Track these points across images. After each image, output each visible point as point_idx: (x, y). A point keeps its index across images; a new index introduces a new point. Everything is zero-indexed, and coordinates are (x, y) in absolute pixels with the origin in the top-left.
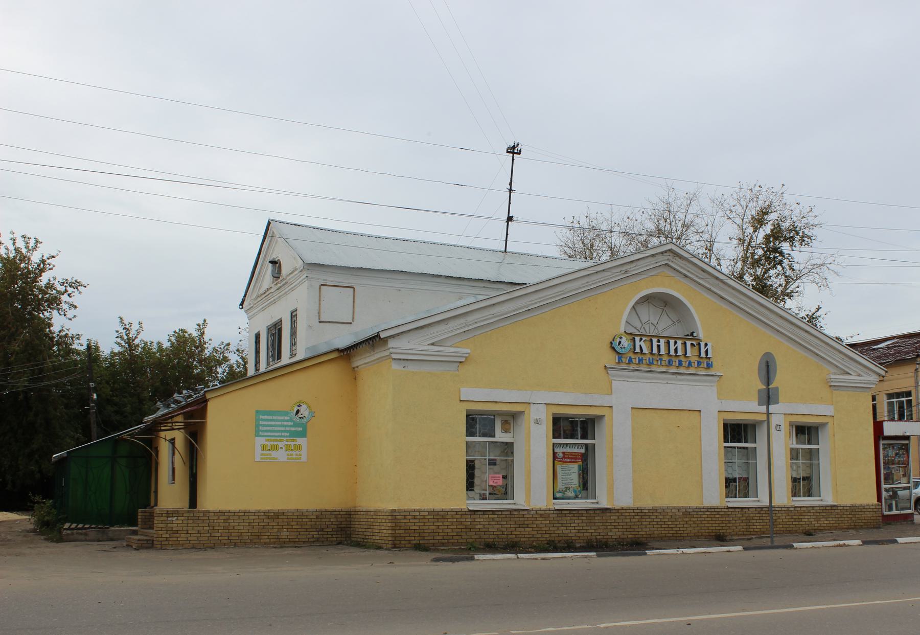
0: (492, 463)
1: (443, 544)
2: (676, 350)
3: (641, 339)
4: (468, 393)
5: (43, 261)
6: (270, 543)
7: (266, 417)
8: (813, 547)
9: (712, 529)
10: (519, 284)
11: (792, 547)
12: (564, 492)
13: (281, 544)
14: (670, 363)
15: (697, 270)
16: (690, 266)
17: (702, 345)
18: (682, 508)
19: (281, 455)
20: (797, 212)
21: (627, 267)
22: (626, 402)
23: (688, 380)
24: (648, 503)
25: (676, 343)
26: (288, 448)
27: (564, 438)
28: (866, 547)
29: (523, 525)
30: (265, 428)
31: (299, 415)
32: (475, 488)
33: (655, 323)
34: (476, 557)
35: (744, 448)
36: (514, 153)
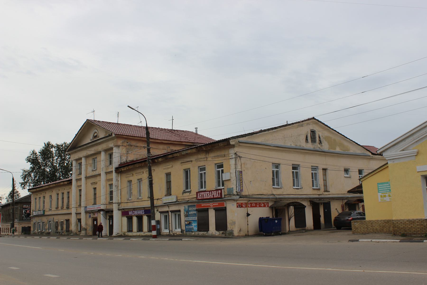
1: (414, 234)
4: (420, 168)
6: (387, 232)
11: (358, 241)
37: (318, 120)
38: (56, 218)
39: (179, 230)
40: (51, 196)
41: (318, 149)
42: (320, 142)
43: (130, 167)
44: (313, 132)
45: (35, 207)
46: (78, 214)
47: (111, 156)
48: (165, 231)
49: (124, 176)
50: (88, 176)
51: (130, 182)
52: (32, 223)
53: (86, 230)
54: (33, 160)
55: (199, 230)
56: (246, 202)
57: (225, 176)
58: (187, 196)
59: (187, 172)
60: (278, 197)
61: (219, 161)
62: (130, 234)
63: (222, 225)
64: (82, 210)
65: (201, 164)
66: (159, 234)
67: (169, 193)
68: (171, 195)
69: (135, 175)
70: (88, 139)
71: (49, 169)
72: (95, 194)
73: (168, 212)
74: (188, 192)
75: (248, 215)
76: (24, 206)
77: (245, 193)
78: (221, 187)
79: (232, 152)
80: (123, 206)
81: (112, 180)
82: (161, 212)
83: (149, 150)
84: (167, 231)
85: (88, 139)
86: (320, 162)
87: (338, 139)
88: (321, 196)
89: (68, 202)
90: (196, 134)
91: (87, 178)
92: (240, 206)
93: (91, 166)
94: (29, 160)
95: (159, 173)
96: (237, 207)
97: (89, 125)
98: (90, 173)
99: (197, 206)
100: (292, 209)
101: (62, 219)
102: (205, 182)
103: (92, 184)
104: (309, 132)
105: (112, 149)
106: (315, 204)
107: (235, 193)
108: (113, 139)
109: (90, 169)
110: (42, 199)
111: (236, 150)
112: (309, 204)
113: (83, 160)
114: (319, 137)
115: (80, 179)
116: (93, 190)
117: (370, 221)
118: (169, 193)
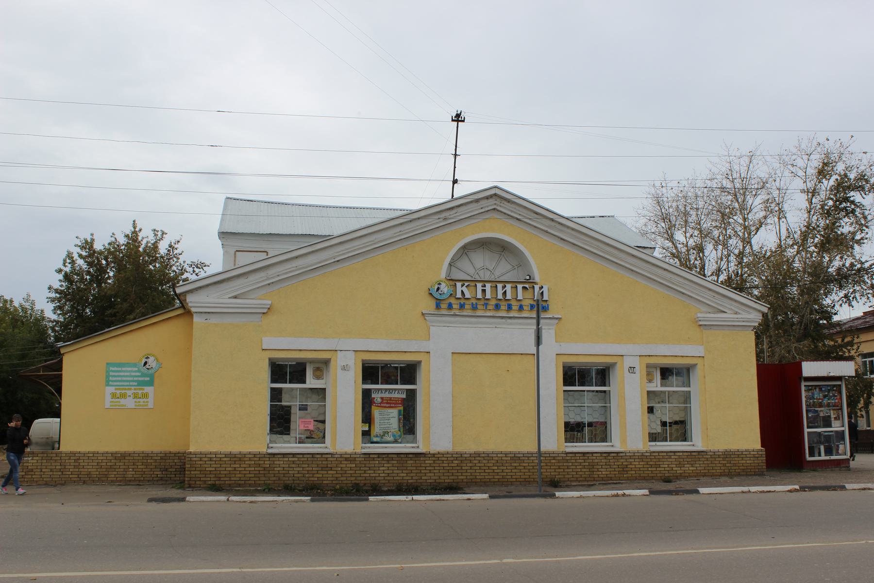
0: (303, 408)
1: (240, 485)
2: (505, 293)
3: (462, 286)
4: (270, 342)
5: (170, 246)
7: (116, 369)
8: (251, 502)
9: (540, 476)
10: (325, 236)
11: (843, 488)
12: (382, 437)
13: (125, 482)
14: (497, 307)
15: (529, 213)
16: (521, 209)
17: (537, 288)
19: (130, 403)
20: (865, 162)
22: (444, 349)
23: (520, 324)
24: (469, 447)
26: (135, 396)
27: (596, 385)
30: (114, 379)
31: (147, 366)
32: (292, 433)
33: (491, 268)
34: (557, 494)
35: (601, 391)
36: (458, 121)
102: (320, 262)
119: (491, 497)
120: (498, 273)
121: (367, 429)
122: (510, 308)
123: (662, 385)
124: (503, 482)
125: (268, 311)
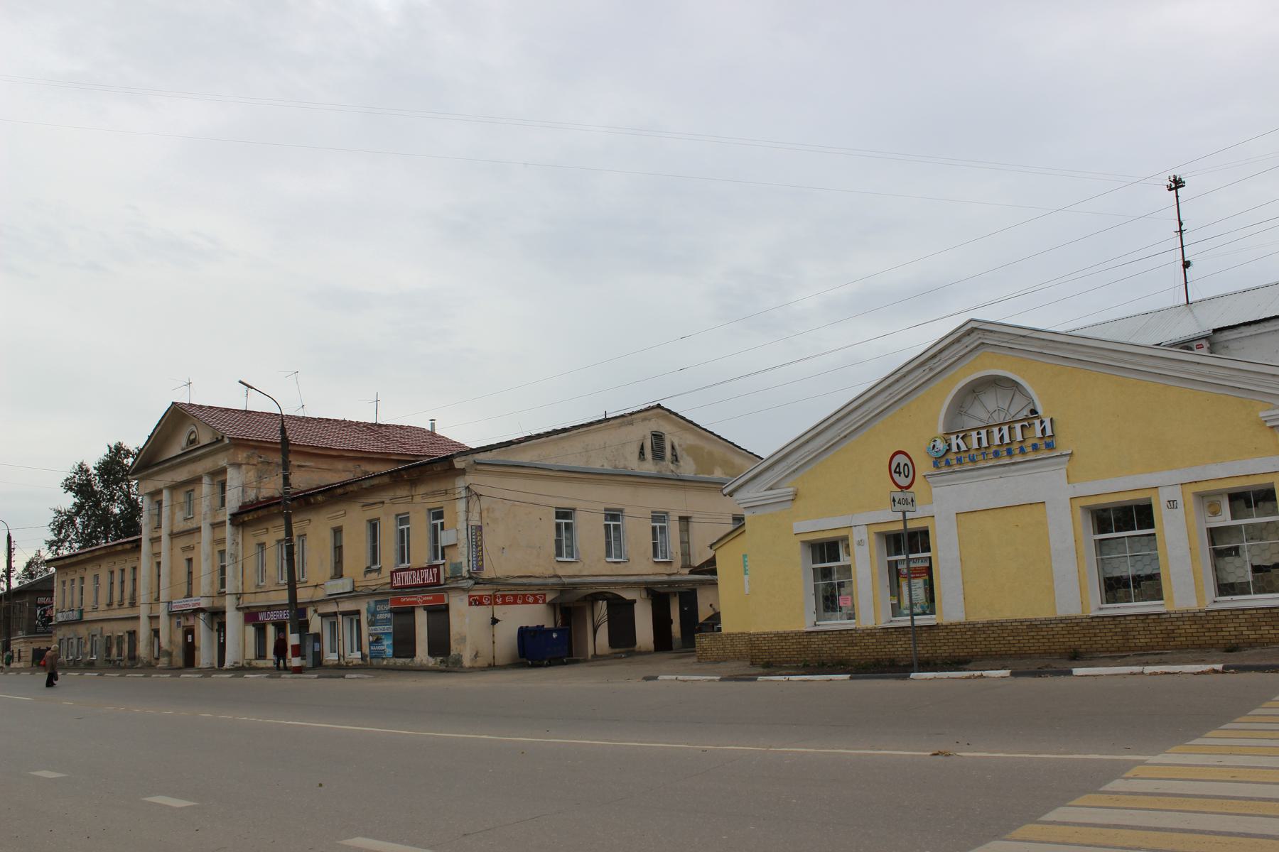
2: (1002, 438)
9: (1042, 649)
11: (655, 678)
18: (1026, 620)
21: (930, 364)
22: (943, 505)
25: (1000, 430)
28: (1232, 677)
29: (853, 644)
37: (669, 411)
38: (109, 629)
39: (358, 655)
40: (97, 577)
41: (669, 474)
42: (675, 459)
43: (260, 513)
44: (658, 437)
45: (62, 603)
46: (153, 618)
47: (223, 485)
48: (330, 658)
49: (250, 532)
50: (175, 530)
51: (262, 545)
52: (55, 639)
53: (169, 654)
54: (80, 486)
55: (396, 655)
56: (491, 593)
57: (445, 538)
58: (374, 581)
59: (374, 525)
60: (566, 580)
61: (435, 503)
62: (261, 663)
63: (440, 644)
64: (162, 610)
65: (401, 509)
66: (318, 662)
67: (338, 574)
68: (341, 576)
69: (271, 530)
70: (176, 449)
71: (106, 507)
72: (190, 573)
73: (335, 614)
74: (375, 570)
75: (495, 621)
76: (40, 600)
77: (486, 574)
78: (440, 561)
79: (461, 483)
80: (249, 601)
81: (223, 541)
82: (323, 616)
83: (286, 479)
84: (334, 657)
85: (176, 449)
86: (674, 502)
87: (718, 450)
88: (673, 578)
89: (134, 590)
90: (433, 434)
91: (173, 536)
92: (477, 602)
93: (182, 509)
94: (69, 487)
95: (315, 531)
96: (470, 604)
97: (177, 416)
98: (181, 526)
99: (394, 601)
100: (602, 606)
101: (120, 629)
103: (184, 549)
104: (649, 436)
105: (223, 471)
106: (659, 597)
107: (465, 574)
108: (226, 448)
109: (179, 515)
110: (77, 583)
111: (469, 479)
112: (644, 594)
113: (165, 495)
114: (673, 448)
115: (158, 539)
116: (185, 564)
117: (729, 635)
118: (338, 574)
119: (1012, 674)
120: (1013, 411)
121: (895, 601)
122: (1010, 453)
123: (1233, 518)
124: (1021, 655)
125: (795, 496)
